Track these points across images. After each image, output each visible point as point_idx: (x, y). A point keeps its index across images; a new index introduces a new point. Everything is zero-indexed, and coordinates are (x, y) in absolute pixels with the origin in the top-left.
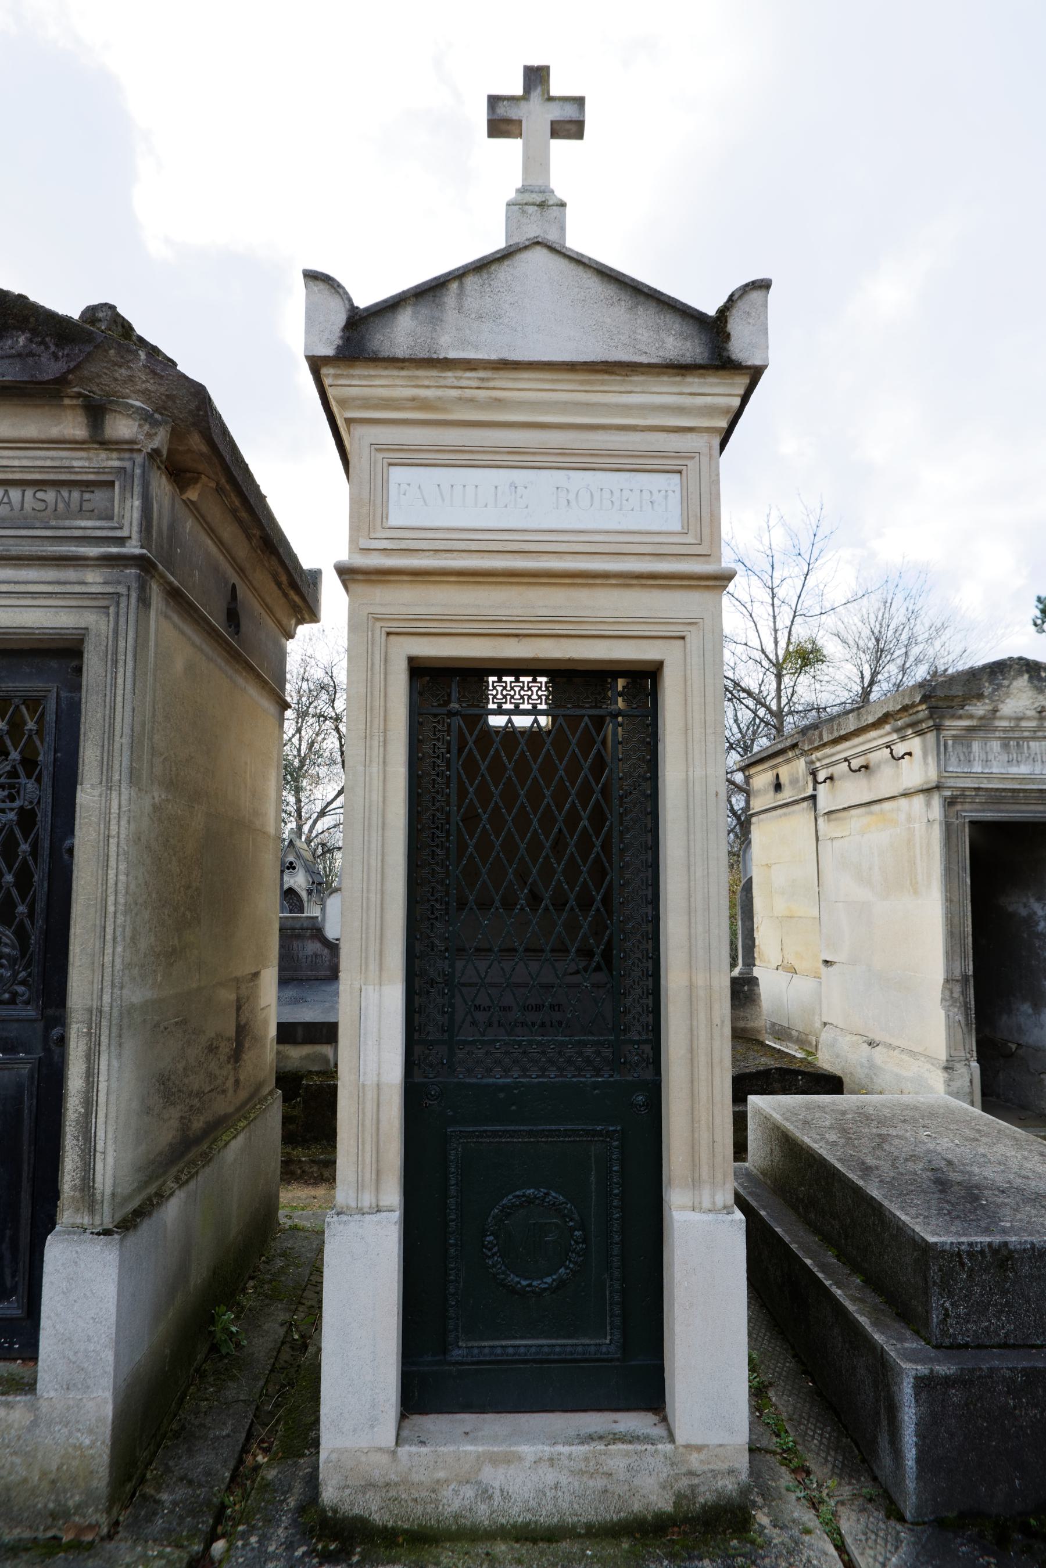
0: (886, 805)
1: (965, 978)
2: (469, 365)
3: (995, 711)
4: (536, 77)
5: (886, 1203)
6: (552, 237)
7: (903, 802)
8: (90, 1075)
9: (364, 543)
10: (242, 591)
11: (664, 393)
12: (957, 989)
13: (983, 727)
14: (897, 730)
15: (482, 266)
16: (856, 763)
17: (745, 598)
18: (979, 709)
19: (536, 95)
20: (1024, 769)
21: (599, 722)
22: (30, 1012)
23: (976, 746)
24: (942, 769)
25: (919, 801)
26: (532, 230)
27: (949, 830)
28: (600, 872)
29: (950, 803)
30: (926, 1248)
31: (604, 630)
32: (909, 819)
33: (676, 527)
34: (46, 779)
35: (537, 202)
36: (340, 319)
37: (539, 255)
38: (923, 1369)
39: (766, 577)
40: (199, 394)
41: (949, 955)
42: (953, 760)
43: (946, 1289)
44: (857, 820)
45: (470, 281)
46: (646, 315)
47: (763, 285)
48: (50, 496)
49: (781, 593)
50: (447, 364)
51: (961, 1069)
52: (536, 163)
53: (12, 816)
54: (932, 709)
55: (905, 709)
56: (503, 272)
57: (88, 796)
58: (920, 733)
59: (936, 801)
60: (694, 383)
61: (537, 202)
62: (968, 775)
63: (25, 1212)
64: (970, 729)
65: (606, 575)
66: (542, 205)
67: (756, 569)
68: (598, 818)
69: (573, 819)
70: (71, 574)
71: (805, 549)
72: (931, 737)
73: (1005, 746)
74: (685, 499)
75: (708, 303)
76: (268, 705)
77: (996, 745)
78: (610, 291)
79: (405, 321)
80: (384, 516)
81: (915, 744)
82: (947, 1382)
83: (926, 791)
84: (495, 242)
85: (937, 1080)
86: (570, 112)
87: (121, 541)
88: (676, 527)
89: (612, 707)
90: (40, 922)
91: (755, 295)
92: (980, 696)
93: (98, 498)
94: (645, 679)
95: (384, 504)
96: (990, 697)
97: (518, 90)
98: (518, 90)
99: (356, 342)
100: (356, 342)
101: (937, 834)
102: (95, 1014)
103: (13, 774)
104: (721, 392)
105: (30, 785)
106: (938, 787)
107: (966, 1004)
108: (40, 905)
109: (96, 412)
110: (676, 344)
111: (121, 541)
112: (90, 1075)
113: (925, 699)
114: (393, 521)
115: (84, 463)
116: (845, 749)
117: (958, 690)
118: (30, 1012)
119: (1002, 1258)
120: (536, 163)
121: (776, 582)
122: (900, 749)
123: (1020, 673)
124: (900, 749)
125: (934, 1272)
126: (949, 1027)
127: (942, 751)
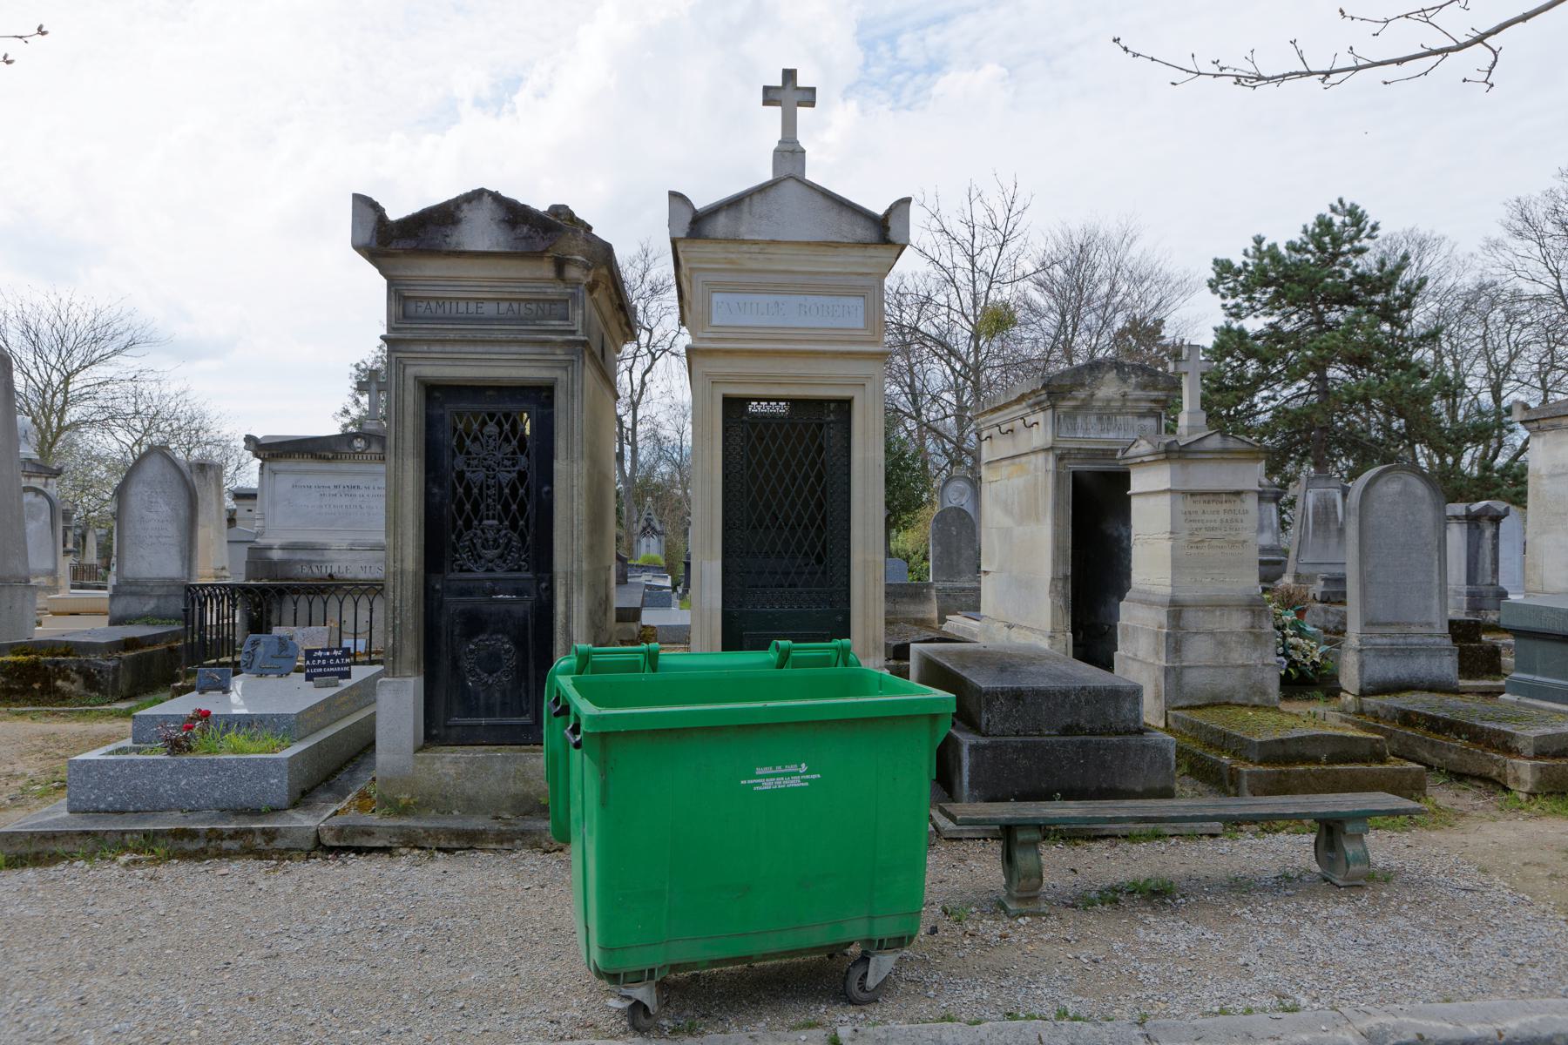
0: (1024, 459)
1: (1066, 577)
2: (755, 242)
3: (1092, 395)
4: (789, 75)
5: (965, 674)
6: (796, 173)
7: (1033, 457)
8: (568, 604)
9: (700, 334)
10: (608, 340)
11: (856, 255)
12: (1060, 585)
13: (1085, 406)
14: (1030, 406)
15: (762, 189)
16: (1004, 428)
17: (948, 264)
18: (1082, 394)
19: (789, 85)
20: (1112, 435)
21: (820, 426)
22: (529, 575)
23: (1079, 420)
24: (1056, 434)
25: (1041, 456)
26: (788, 169)
27: (1058, 477)
28: (820, 505)
29: (1060, 458)
30: (979, 690)
31: (822, 382)
32: (1036, 469)
33: (861, 325)
34: (532, 455)
35: (789, 153)
36: (689, 218)
37: (791, 184)
38: (973, 742)
39: (967, 245)
40: (608, 248)
41: (1055, 562)
42: (1064, 429)
43: (989, 710)
44: (1006, 469)
45: (756, 198)
46: (847, 216)
47: (907, 201)
48: (533, 306)
49: (979, 262)
50: (744, 241)
51: (1060, 636)
52: (789, 124)
53: (515, 475)
54: (1050, 394)
55: (1033, 392)
56: (772, 193)
57: (559, 465)
58: (1043, 410)
59: (1051, 458)
60: (871, 251)
61: (789, 153)
62: (1073, 439)
63: (532, 673)
64: (1076, 408)
65: (824, 353)
66: (793, 152)
67: (959, 238)
68: (819, 477)
69: (806, 478)
70: (547, 350)
71: (1000, 223)
72: (1050, 412)
73: (1100, 419)
74: (866, 313)
75: (880, 211)
76: (612, 400)
77: (1093, 419)
78: (827, 203)
79: (722, 221)
80: (710, 320)
81: (1040, 417)
82: (985, 747)
83: (1046, 450)
84: (767, 175)
85: (1044, 644)
86: (808, 96)
87: (573, 332)
88: (861, 325)
89: (823, 422)
90: (532, 530)
91: (903, 206)
92: (1083, 385)
93: (558, 308)
94: (845, 405)
95: (710, 314)
96: (1090, 385)
97: (779, 83)
98: (779, 83)
99: (695, 226)
100: (695, 226)
101: (1050, 480)
102: (569, 575)
103: (514, 453)
104: (883, 253)
105: (523, 459)
106: (1052, 448)
107: (1065, 596)
108: (531, 521)
109: (560, 264)
110: (862, 232)
111: (573, 332)
112: (568, 604)
113: (1044, 386)
114: (714, 323)
115: (555, 291)
116: (998, 417)
117: (1067, 381)
118: (529, 575)
119: (1017, 696)
120: (789, 124)
121: (977, 251)
122: (1030, 419)
123: (1111, 369)
124: (1030, 419)
125: (983, 701)
126: (1053, 610)
127: (1056, 422)
